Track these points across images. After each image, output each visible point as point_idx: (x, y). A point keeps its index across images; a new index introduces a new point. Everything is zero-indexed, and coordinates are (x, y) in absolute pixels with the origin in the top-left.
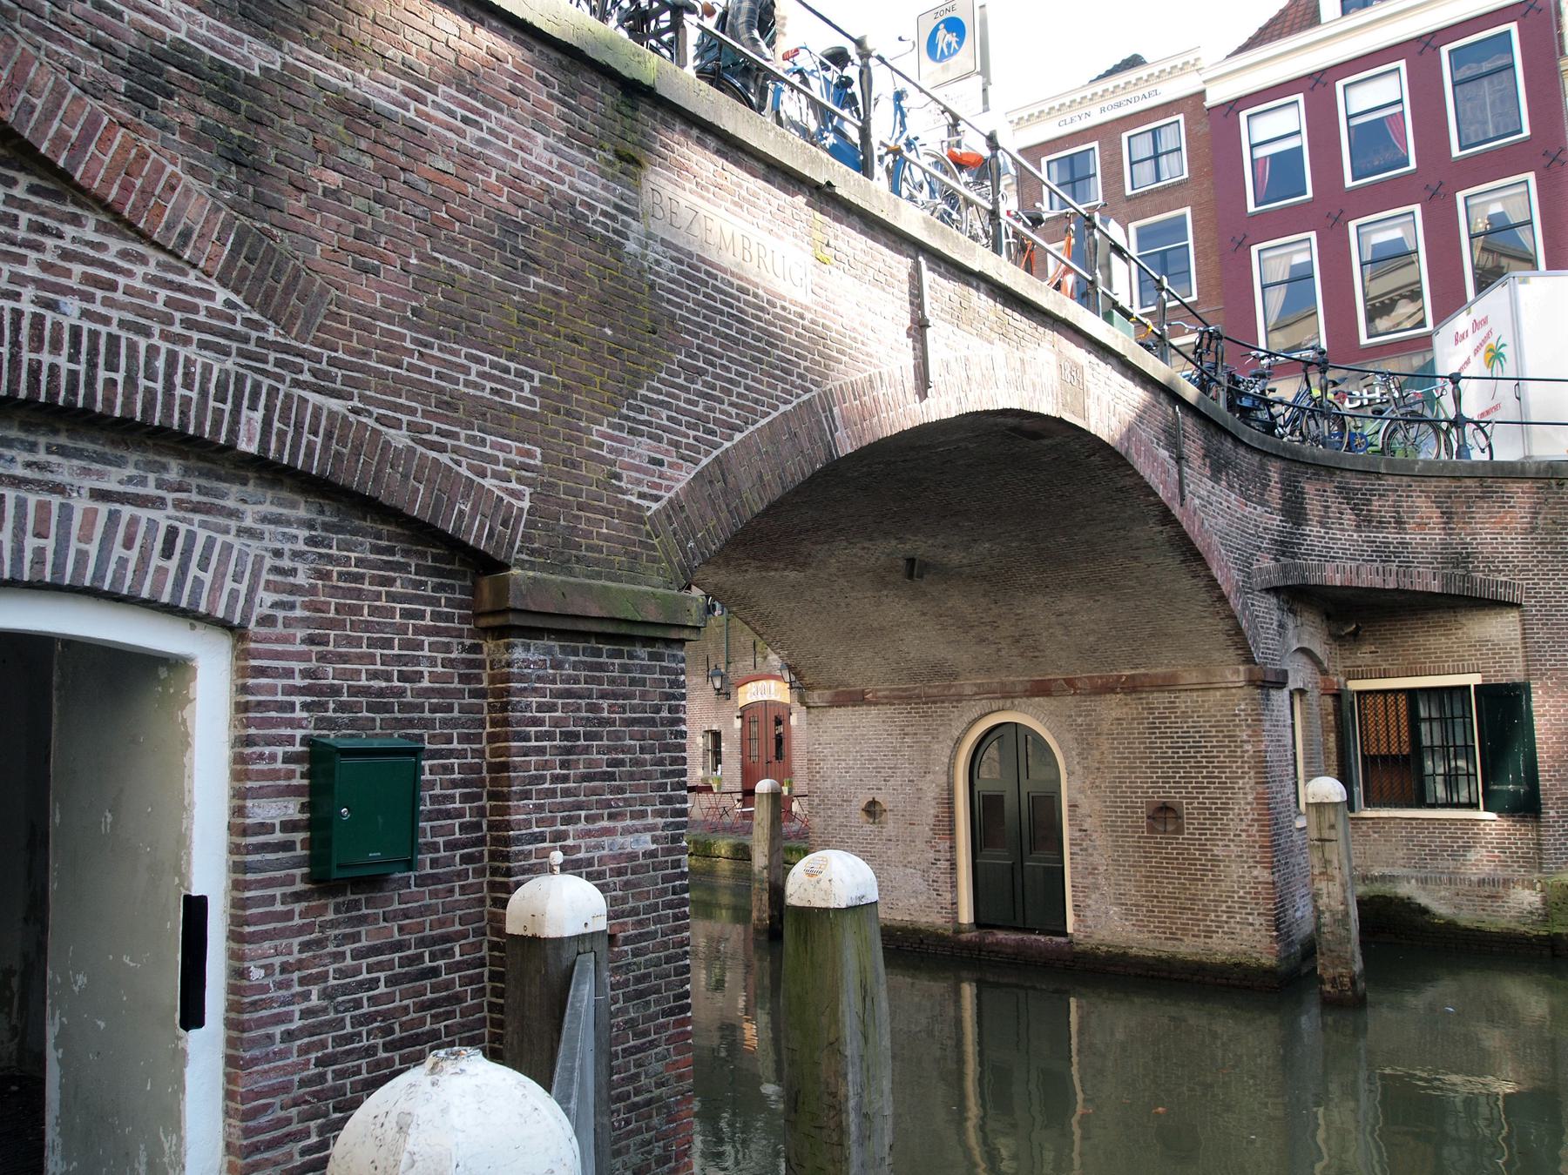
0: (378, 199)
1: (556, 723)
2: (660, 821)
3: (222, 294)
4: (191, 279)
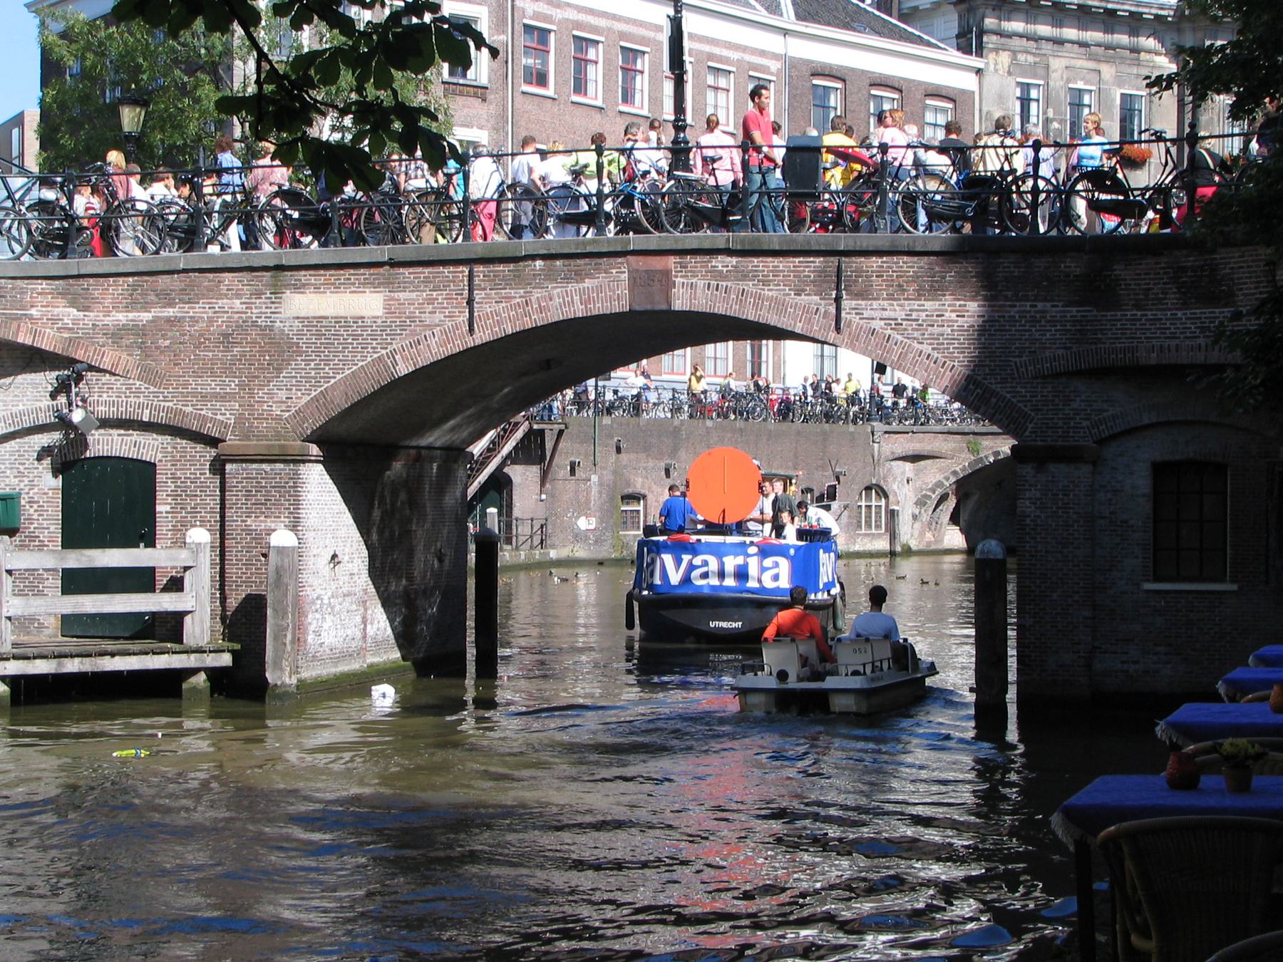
0: (181, 343)
1: (243, 487)
2: (287, 520)
3: (138, 383)
4: (131, 381)
